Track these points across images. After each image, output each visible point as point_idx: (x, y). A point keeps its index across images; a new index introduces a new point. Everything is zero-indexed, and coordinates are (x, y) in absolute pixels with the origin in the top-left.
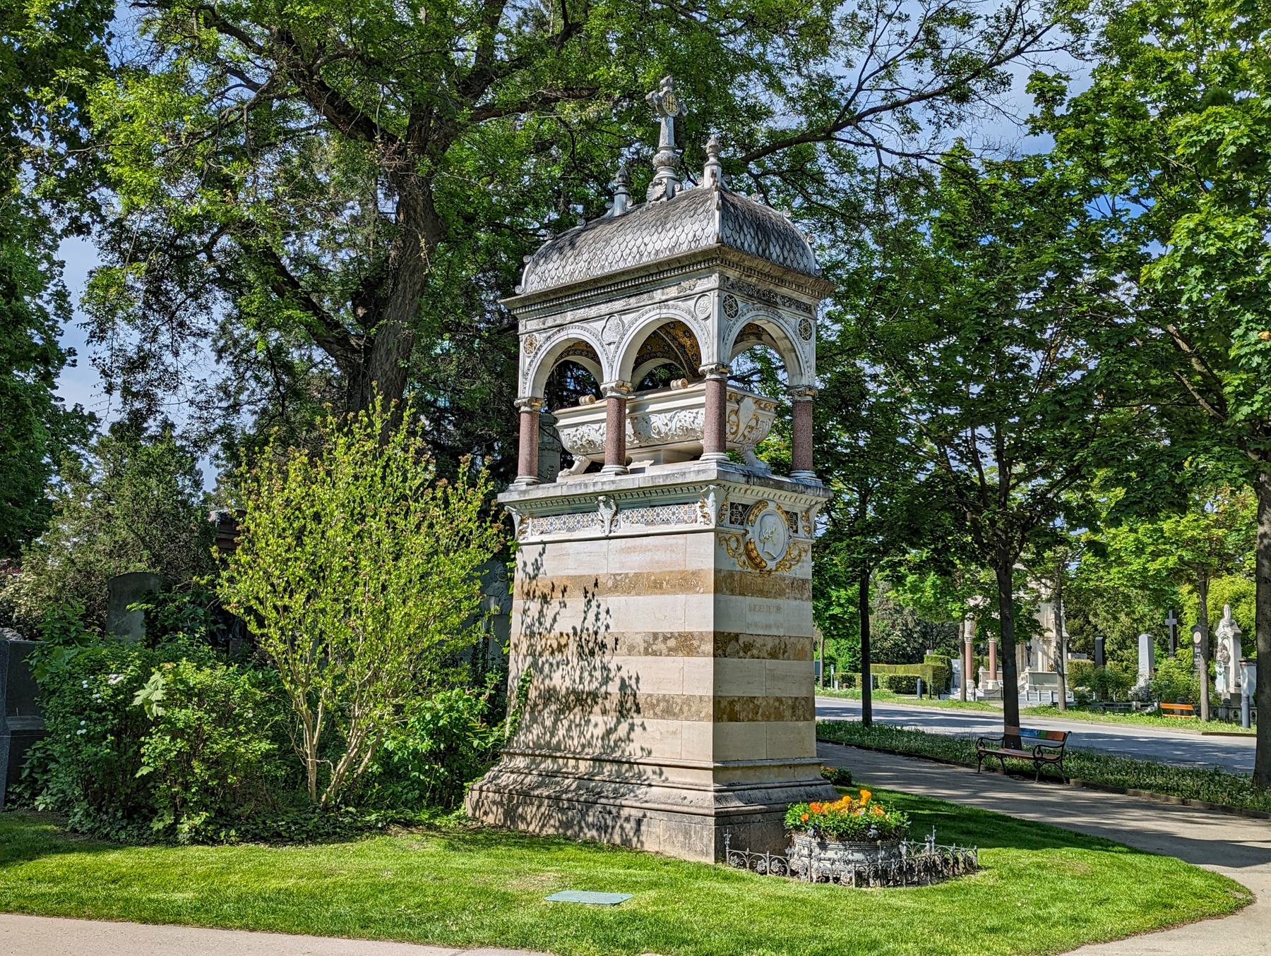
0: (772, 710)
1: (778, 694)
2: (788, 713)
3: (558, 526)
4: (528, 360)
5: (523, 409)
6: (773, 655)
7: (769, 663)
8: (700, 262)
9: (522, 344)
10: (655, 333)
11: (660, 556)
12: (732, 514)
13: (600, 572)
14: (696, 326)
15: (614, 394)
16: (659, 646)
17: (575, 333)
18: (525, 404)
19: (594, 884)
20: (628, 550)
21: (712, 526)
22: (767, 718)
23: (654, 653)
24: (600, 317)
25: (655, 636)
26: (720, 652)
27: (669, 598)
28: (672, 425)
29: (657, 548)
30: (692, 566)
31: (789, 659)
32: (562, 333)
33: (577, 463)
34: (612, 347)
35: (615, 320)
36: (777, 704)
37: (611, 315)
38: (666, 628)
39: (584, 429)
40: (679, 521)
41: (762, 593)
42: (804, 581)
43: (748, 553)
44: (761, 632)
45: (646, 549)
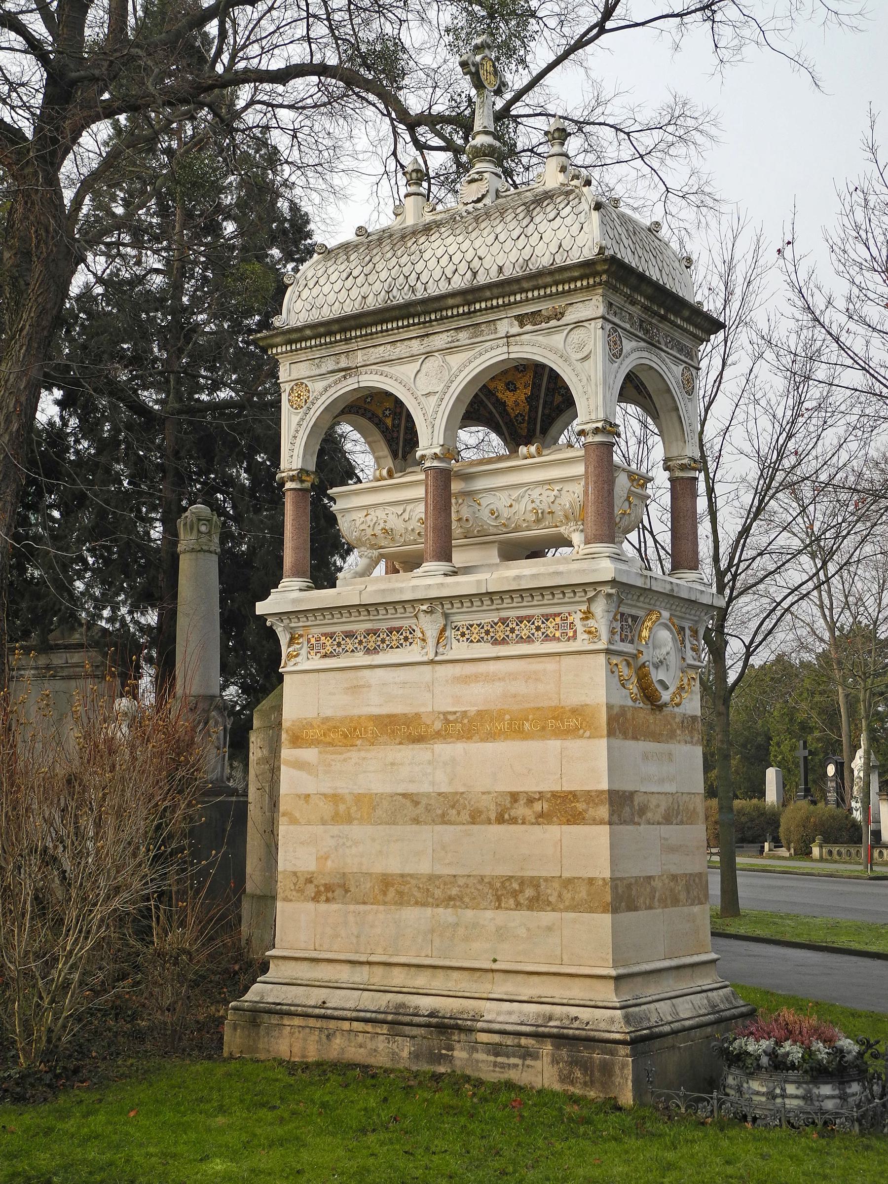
0: (668, 893)
1: (674, 870)
2: (683, 896)
4: (295, 419)
5: (289, 485)
6: (667, 819)
8: (311, 339)
9: (284, 398)
11: (520, 687)
13: (422, 710)
14: (568, 370)
15: (436, 464)
16: (521, 810)
17: (370, 380)
18: (292, 479)
20: (466, 680)
21: (602, 645)
22: (664, 904)
23: (513, 821)
24: (413, 357)
25: (514, 797)
26: (615, 818)
27: (534, 746)
28: (520, 507)
29: (513, 676)
30: (573, 698)
32: (350, 381)
34: (433, 400)
35: (433, 363)
38: (531, 786)
39: (380, 513)
40: (547, 638)
41: (655, 737)
42: (694, 718)
44: (655, 790)
45: (489, 678)
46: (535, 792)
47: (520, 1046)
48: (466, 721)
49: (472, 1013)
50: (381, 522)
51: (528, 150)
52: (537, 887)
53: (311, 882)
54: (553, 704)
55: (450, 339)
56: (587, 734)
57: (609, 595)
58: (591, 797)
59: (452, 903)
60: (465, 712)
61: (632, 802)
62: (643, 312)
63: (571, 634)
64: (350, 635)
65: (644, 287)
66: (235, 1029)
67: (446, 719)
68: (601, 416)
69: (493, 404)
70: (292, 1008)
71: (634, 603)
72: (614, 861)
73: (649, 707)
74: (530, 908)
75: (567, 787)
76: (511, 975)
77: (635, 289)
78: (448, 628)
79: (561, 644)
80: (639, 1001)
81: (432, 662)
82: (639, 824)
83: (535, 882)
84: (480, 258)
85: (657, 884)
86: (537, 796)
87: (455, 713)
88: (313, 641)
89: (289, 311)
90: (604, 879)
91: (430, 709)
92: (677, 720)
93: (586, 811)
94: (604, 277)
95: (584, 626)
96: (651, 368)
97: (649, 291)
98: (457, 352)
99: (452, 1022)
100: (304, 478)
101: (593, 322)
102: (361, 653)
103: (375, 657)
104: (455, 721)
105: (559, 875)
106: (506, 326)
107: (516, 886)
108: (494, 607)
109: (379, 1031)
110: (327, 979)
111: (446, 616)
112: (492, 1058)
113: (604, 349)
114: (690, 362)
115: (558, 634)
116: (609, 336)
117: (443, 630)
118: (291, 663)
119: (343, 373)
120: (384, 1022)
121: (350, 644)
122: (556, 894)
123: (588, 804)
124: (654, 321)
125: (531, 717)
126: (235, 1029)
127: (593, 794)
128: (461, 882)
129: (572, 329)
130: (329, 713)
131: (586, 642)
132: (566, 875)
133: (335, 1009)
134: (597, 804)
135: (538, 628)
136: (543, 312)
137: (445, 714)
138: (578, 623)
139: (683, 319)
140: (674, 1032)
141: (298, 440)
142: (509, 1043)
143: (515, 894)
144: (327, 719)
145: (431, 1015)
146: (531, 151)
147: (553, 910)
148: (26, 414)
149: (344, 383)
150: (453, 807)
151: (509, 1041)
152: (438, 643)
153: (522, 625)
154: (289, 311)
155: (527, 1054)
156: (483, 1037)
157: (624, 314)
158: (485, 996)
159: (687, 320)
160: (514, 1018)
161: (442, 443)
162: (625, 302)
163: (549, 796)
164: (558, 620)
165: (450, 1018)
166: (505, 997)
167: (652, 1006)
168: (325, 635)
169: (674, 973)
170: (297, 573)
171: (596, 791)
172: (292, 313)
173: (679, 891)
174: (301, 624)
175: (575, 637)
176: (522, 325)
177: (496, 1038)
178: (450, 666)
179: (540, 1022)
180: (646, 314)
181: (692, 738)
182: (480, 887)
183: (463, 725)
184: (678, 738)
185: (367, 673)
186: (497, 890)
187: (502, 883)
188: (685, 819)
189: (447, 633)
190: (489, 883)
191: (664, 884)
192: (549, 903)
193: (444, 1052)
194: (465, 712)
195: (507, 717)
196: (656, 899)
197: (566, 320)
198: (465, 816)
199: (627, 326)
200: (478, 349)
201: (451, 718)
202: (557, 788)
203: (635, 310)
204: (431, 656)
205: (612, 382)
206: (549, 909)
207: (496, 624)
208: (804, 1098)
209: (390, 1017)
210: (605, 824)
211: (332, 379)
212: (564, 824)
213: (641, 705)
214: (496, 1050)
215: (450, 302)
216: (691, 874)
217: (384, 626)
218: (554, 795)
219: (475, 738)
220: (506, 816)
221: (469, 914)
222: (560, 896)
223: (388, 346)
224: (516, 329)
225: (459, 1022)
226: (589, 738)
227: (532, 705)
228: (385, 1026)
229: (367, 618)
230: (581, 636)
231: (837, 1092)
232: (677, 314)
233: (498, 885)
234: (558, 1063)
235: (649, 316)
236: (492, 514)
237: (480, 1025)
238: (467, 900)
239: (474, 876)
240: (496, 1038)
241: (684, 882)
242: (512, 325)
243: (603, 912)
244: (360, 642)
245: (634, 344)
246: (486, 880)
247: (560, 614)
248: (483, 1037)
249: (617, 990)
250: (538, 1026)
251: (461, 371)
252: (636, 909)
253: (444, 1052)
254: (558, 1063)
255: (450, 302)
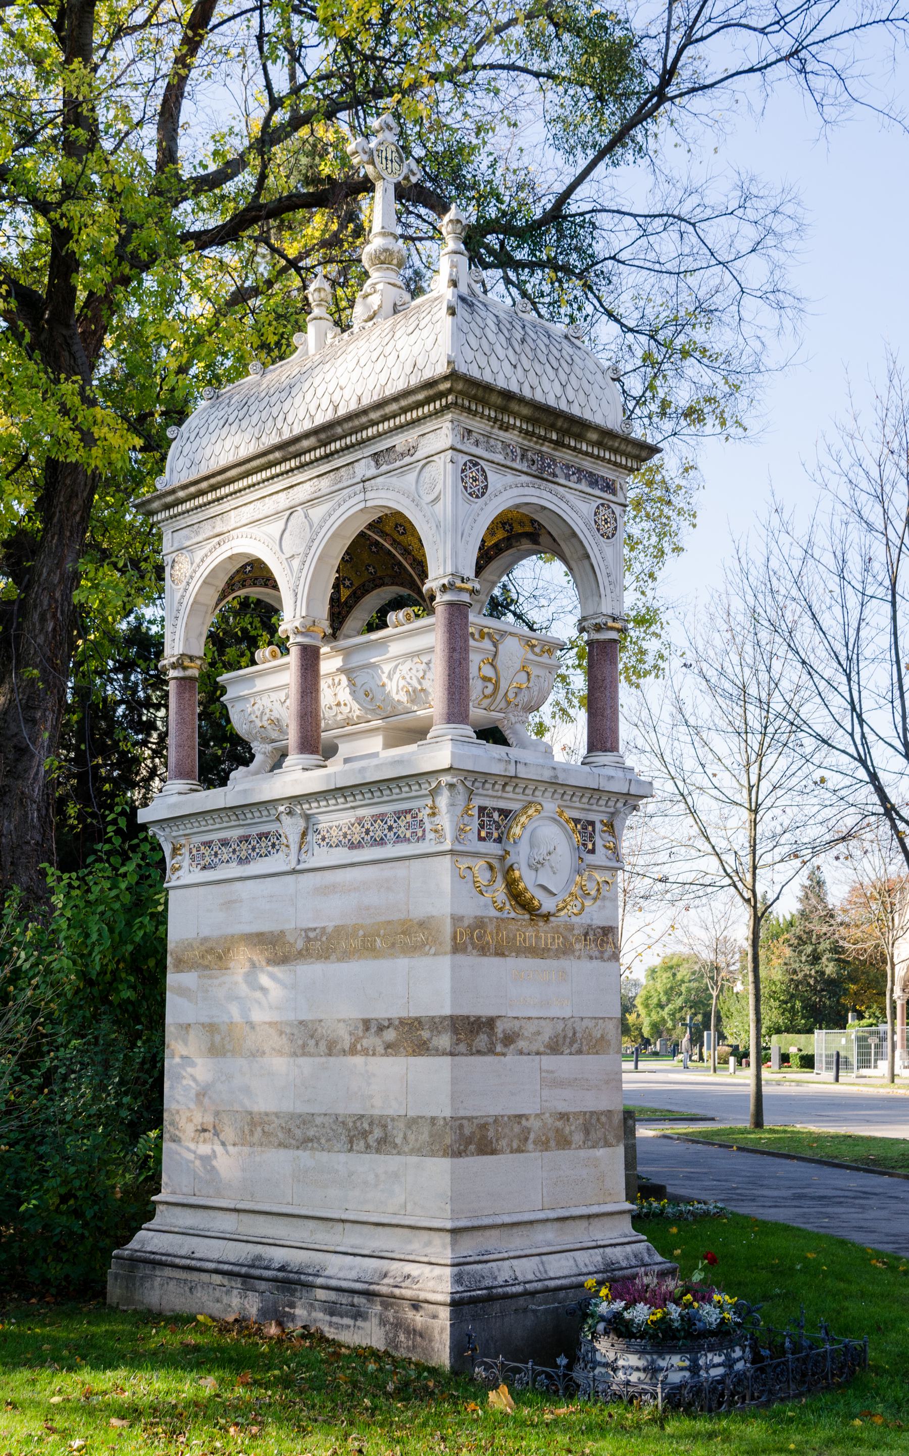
0: (551, 1134)
1: (563, 1107)
2: (578, 1138)
3: (225, 857)
5: (172, 673)
6: (554, 1048)
7: (549, 1062)
10: (362, 535)
12: (482, 826)
18: (174, 666)
19: (799, 1083)
20: (326, 890)
22: (544, 1145)
25: (367, 1023)
27: (384, 965)
30: (421, 909)
31: (580, 1052)
32: (224, 547)
33: (258, 758)
36: (559, 1124)
37: (292, 510)
38: (381, 1012)
40: (399, 839)
43: (512, 886)
44: (533, 1014)
46: (384, 1019)
47: (353, 1305)
48: (324, 939)
49: (318, 1268)
50: (267, 711)
51: (610, 258)
52: (385, 1126)
53: (191, 1121)
54: (403, 917)
55: (313, 489)
56: (433, 951)
57: (451, 786)
58: (435, 1024)
59: (310, 1145)
60: (324, 928)
61: (492, 1029)
62: (524, 438)
63: (420, 834)
64: (225, 843)
65: (514, 406)
66: (116, 1279)
67: (307, 937)
68: (449, 570)
69: (411, 565)
70: (164, 1258)
71: (499, 794)
72: (455, 1097)
73: (527, 916)
74: (378, 1151)
75: (413, 1014)
76: (358, 1226)
77: (504, 410)
78: (310, 831)
79: (411, 845)
80: (485, 1258)
81: (294, 872)
82: (504, 1055)
83: (382, 1122)
84: (341, 389)
85: (534, 1124)
86: (386, 1024)
87: (315, 929)
88: (194, 852)
89: (172, 471)
90: (444, 1118)
91: (293, 926)
92: (576, 932)
93: (430, 1040)
94: (450, 398)
95: (431, 823)
96: (544, 508)
97: (525, 411)
98: (319, 504)
99: (296, 1276)
100: (186, 664)
101: (442, 455)
102: (235, 864)
103: (247, 867)
104: (316, 939)
105: (403, 1113)
106: (366, 468)
107: (366, 1126)
108: (348, 805)
109: (233, 1284)
110: (201, 1227)
111: (307, 817)
112: (328, 1318)
113: (455, 487)
114: (611, 497)
115: (408, 835)
116: (463, 471)
117: (304, 834)
118: (174, 877)
119: (217, 539)
120: (238, 1275)
121: (225, 853)
122: (401, 1135)
123: (432, 1031)
124: (544, 449)
125: (382, 932)
126: (116, 1279)
127: (437, 1020)
128: (319, 1120)
129: (424, 466)
130: (206, 932)
131: (433, 842)
132: (411, 1114)
133: (200, 1260)
134: (439, 1032)
135: (390, 828)
136: (397, 448)
137: (306, 930)
138: (426, 820)
139: (594, 444)
140: (526, 1293)
141: (179, 622)
142: (344, 1302)
143: (365, 1134)
144: (205, 940)
145: (282, 1269)
146: (613, 258)
147: (399, 1153)
148: (62, 612)
149: (219, 551)
150: (312, 1037)
151: (344, 1299)
152: (300, 849)
153: (376, 826)
154: (172, 471)
155: (358, 1315)
156: (321, 1294)
157: (492, 442)
158: (332, 1248)
159: (599, 444)
160: (353, 1275)
161: (304, 614)
162: (492, 427)
163: (397, 1023)
164: (409, 816)
165: (296, 1273)
166: (350, 1251)
167: (507, 1263)
168: (204, 844)
169: (557, 1225)
170: (182, 774)
171: (440, 1017)
172: (175, 473)
173: (571, 1132)
174: (181, 833)
175: (423, 837)
176: (378, 465)
177: (332, 1296)
178: (311, 874)
179: (376, 1279)
180: (530, 441)
181: (602, 952)
182: (334, 1127)
183: (323, 942)
184: (577, 954)
185: (238, 885)
186: (349, 1131)
187: (354, 1122)
188: (585, 1048)
189: (309, 838)
190: (343, 1123)
191: (545, 1124)
192: (395, 1146)
193: (287, 1309)
194: (324, 928)
195: (361, 933)
196: (530, 1141)
197: (419, 455)
198: (323, 1046)
199: (499, 458)
200: (337, 499)
201: (312, 935)
202: (404, 1014)
203: (512, 437)
204: (293, 865)
205: (467, 528)
206: (395, 1152)
207: (353, 825)
208: (645, 1370)
209: (244, 1270)
210: (447, 1054)
211: (209, 547)
212: (410, 1055)
213: (513, 915)
214: (332, 1309)
215: (305, 444)
216: (592, 1113)
217: (254, 831)
218: (402, 1022)
219: (333, 957)
220: (359, 1047)
221: (324, 1157)
222: (405, 1138)
223: (258, 503)
224: (373, 471)
225: (302, 1277)
226: (435, 954)
227: (383, 918)
228: (239, 1279)
229: (237, 823)
230: (430, 835)
231: (687, 1363)
232: (580, 437)
233: (351, 1124)
234: (385, 1325)
235: (536, 443)
236: (367, 695)
237: (320, 1281)
238: (323, 1141)
239: (330, 1115)
240: (332, 1296)
241: (581, 1121)
242: (369, 467)
243: (444, 1156)
244: (234, 851)
245: (510, 478)
246: (340, 1119)
247: (410, 810)
248: (321, 1294)
249: (454, 1243)
250: (371, 1283)
251: (321, 527)
252: (493, 1152)
253: (287, 1309)
254: (385, 1325)
255: (305, 444)
